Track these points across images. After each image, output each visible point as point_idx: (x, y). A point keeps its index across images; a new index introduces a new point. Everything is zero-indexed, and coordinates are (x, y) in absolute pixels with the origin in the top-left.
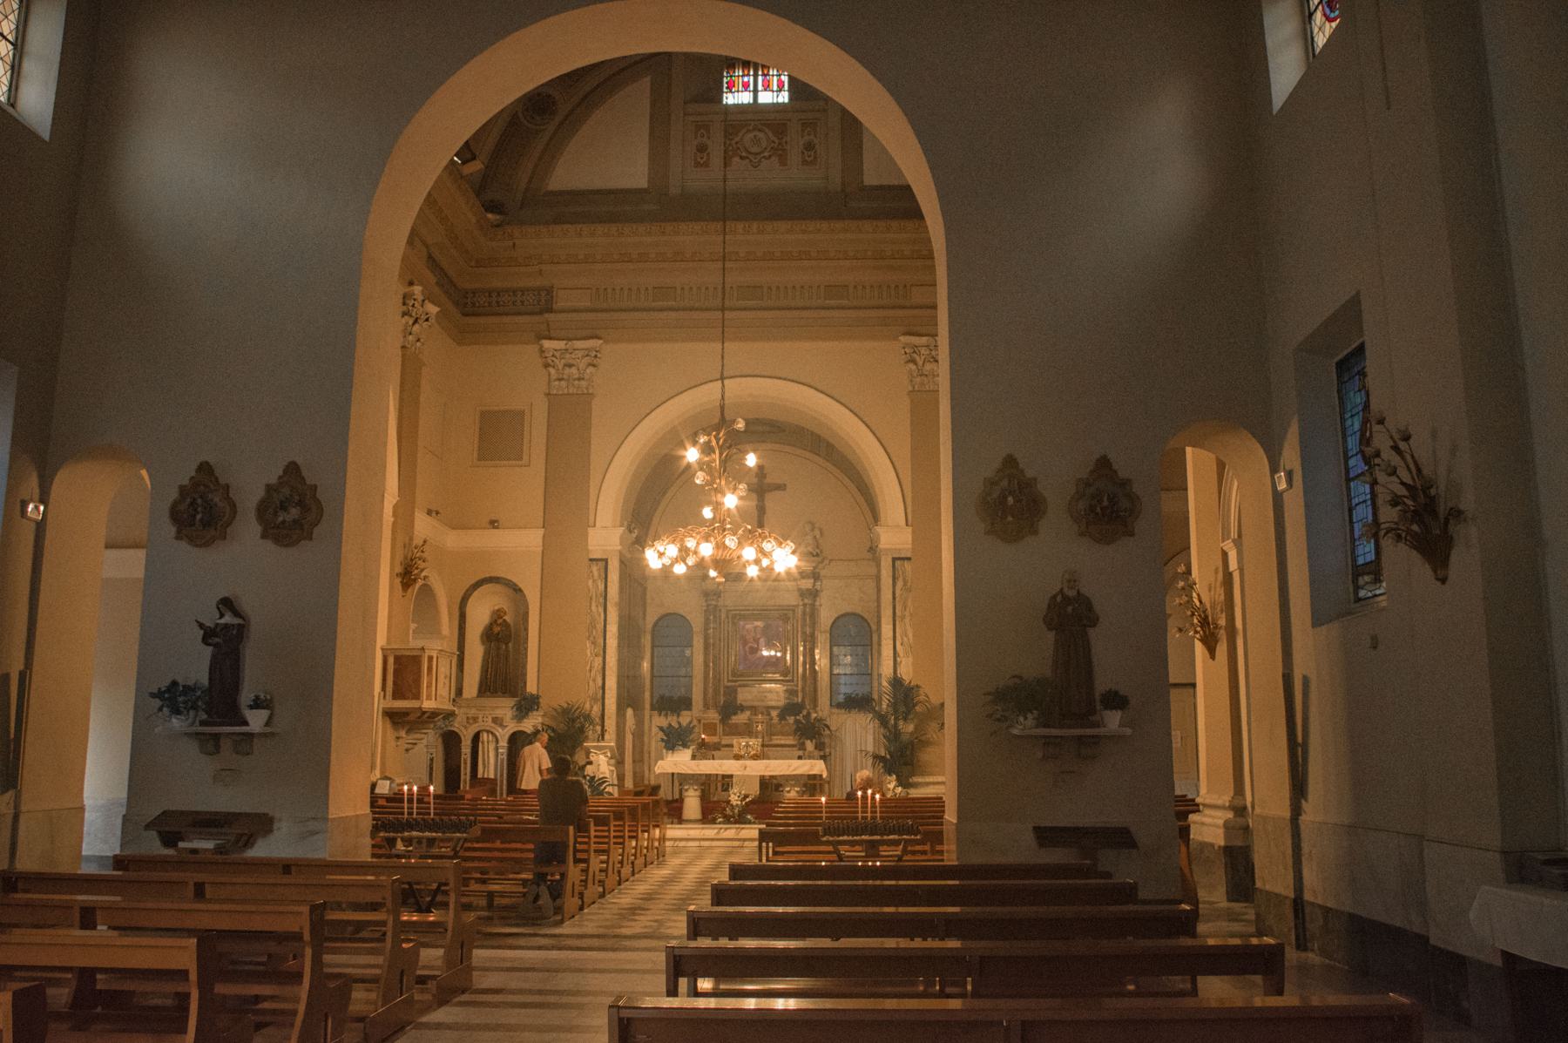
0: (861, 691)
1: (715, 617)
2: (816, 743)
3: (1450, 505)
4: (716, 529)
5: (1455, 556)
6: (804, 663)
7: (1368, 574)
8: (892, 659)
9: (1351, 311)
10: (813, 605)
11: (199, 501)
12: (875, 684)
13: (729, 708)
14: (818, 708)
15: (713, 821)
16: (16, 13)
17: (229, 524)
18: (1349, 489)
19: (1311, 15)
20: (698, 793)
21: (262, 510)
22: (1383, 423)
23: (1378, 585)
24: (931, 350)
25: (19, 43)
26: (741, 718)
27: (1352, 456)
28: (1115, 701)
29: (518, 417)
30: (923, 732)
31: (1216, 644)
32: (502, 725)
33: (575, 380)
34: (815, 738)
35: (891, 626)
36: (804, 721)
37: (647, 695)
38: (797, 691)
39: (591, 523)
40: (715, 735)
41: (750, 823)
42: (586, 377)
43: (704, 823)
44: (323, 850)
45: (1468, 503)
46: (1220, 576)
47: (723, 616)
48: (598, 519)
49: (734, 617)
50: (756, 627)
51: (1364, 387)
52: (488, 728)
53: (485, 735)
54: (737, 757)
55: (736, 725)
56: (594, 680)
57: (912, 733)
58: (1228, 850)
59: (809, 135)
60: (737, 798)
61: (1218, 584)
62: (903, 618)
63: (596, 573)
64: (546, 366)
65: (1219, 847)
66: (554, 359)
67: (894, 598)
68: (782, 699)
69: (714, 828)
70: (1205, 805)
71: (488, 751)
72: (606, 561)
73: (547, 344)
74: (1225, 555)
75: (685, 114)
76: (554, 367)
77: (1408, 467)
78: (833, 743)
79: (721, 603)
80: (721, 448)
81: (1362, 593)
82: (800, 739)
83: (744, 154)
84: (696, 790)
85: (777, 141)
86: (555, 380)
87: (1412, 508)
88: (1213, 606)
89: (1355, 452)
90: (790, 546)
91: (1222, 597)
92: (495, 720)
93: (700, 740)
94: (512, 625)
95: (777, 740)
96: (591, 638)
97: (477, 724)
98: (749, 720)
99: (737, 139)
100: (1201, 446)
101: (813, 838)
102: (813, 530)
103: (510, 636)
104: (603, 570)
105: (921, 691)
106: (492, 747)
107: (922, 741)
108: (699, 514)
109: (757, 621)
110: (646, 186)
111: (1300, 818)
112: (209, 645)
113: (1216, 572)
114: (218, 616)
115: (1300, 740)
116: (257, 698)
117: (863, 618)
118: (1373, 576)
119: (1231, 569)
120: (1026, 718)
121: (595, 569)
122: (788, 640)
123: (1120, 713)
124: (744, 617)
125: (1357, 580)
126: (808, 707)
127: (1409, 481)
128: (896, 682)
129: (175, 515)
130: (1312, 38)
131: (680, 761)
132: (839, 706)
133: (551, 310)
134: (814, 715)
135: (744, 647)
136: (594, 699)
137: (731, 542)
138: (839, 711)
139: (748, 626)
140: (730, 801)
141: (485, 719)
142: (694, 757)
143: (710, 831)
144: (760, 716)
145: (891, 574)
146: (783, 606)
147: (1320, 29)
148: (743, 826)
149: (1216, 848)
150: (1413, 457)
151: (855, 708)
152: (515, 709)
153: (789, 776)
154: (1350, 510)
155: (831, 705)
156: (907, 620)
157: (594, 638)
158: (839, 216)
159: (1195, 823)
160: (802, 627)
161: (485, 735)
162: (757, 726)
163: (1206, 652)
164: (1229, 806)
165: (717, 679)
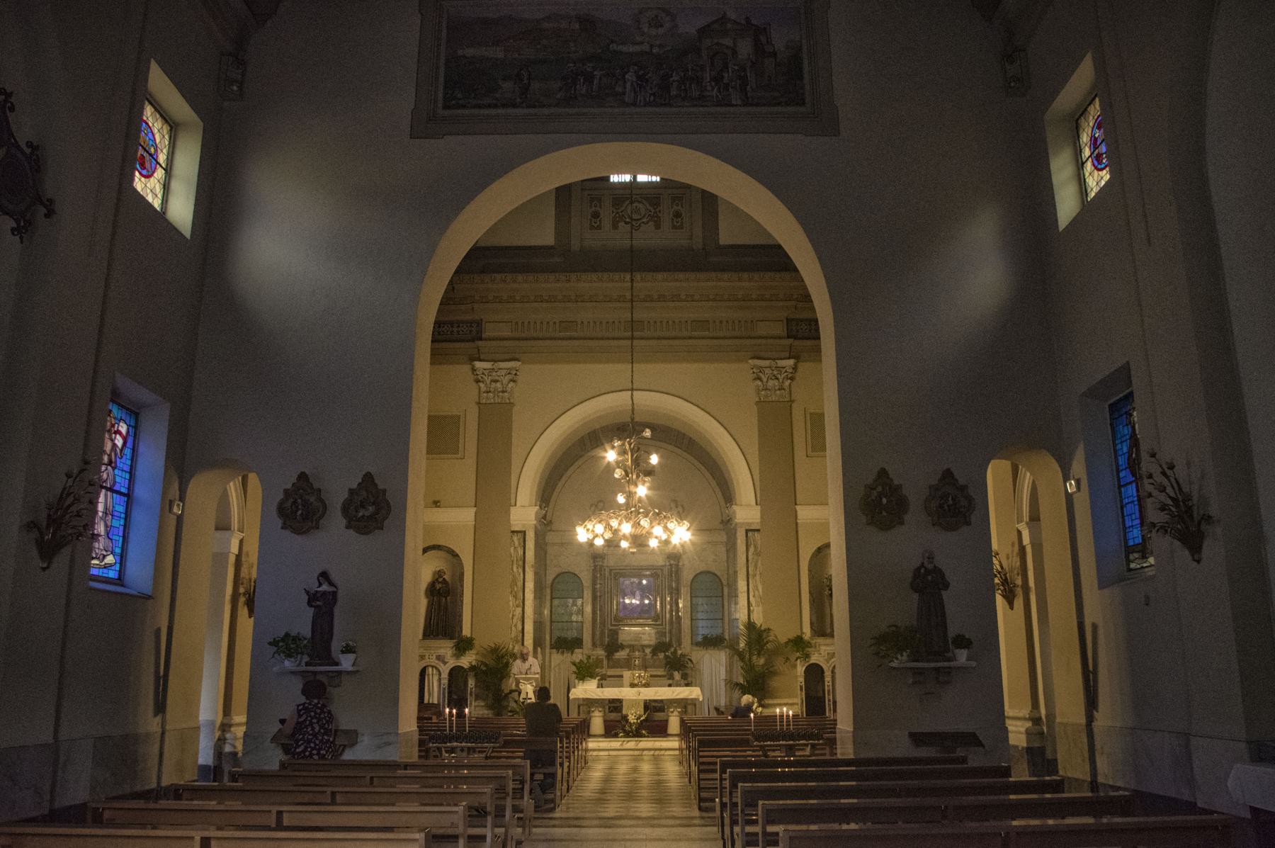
0: (716, 632)
1: (601, 575)
3: (1202, 512)
4: (633, 510)
5: (1207, 545)
6: (671, 611)
7: (1136, 552)
9: (1124, 373)
11: (299, 501)
12: (727, 627)
13: (613, 646)
14: (682, 646)
15: (616, 736)
16: (167, 147)
18: (1120, 493)
19: (1083, 164)
20: (601, 714)
21: (345, 510)
22: (1154, 457)
23: (1145, 560)
24: (773, 370)
25: (169, 169)
26: (622, 654)
27: (1122, 470)
28: (962, 642)
29: (455, 420)
31: (1014, 599)
32: (445, 663)
33: (499, 392)
36: (672, 657)
37: (548, 637)
38: (665, 633)
39: (513, 501)
41: (645, 737)
42: (509, 390)
43: (606, 737)
44: (392, 755)
45: (1214, 510)
46: (1016, 548)
47: (607, 574)
48: (518, 498)
49: (616, 574)
50: (632, 583)
51: (1130, 422)
52: (433, 664)
53: (430, 669)
56: (516, 626)
58: (1029, 750)
59: (678, 206)
60: (633, 717)
61: (1015, 554)
62: (755, 575)
64: (478, 381)
65: (1023, 748)
66: (482, 376)
67: (747, 561)
68: (654, 639)
69: (619, 741)
71: (433, 683)
72: (524, 532)
73: (478, 364)
74: (1019, 533)
75: (582, 189)
76: (483, 382)
77: (1171, 484)
78: (694, 674)
80: (632, 450)
81: (1133, 566)
83: (628, 220)
84: (600, 711)
85: (653, 211)
86: (484, 392)
87: (1176, 514)
89: (1124, 467)
90: (686, 524)
91: (1018, 563)
92: (438, 658)
94: (450, 582)
96: (513, 593)
97: (424, 661)
99: (623, 208)
101: (745, 743)
103: (449, 591)
104: (522, 540)
106: (436, 678)
107: (771, 672)
108: (616, 502)
110: (553, 244)
111: (1093, 724)
112: (312, 606)
113: (1013, 544)
114: (317, 584)
115: (1091, 668)
116: (348, 645)
118: (1141, 554)
119: (1025, 543)
120: (902, 656)
121: (515, 539)
122: (659, 594)
123: (967, 650)
124: (623, 575)
125: (1129, 556)
127: (1172, 494)
128: (750, 626)
129: (281, 510)
130: (1085, 180)
131: (587, 689)
132: (698, 644)
133: (481, 339)
134: (679, 652)
137: (645, 522)
138: (698, 648)
139: (627, 582)
141: (431, 657)
143: (615, 743)
144: (637, 653)
147: (1090, 174)
148: (641, 739)
149: (1020, 749)
150: (1176, 479)
152: (454, 648)
153: (674, 699)
154: (1122, 508)
156: (758, 577)
157: (516, 592)
158: (699, 270)
161: (430, 669)
163: (1006, 603)
164: (1029, 717)
165: (603, 623)
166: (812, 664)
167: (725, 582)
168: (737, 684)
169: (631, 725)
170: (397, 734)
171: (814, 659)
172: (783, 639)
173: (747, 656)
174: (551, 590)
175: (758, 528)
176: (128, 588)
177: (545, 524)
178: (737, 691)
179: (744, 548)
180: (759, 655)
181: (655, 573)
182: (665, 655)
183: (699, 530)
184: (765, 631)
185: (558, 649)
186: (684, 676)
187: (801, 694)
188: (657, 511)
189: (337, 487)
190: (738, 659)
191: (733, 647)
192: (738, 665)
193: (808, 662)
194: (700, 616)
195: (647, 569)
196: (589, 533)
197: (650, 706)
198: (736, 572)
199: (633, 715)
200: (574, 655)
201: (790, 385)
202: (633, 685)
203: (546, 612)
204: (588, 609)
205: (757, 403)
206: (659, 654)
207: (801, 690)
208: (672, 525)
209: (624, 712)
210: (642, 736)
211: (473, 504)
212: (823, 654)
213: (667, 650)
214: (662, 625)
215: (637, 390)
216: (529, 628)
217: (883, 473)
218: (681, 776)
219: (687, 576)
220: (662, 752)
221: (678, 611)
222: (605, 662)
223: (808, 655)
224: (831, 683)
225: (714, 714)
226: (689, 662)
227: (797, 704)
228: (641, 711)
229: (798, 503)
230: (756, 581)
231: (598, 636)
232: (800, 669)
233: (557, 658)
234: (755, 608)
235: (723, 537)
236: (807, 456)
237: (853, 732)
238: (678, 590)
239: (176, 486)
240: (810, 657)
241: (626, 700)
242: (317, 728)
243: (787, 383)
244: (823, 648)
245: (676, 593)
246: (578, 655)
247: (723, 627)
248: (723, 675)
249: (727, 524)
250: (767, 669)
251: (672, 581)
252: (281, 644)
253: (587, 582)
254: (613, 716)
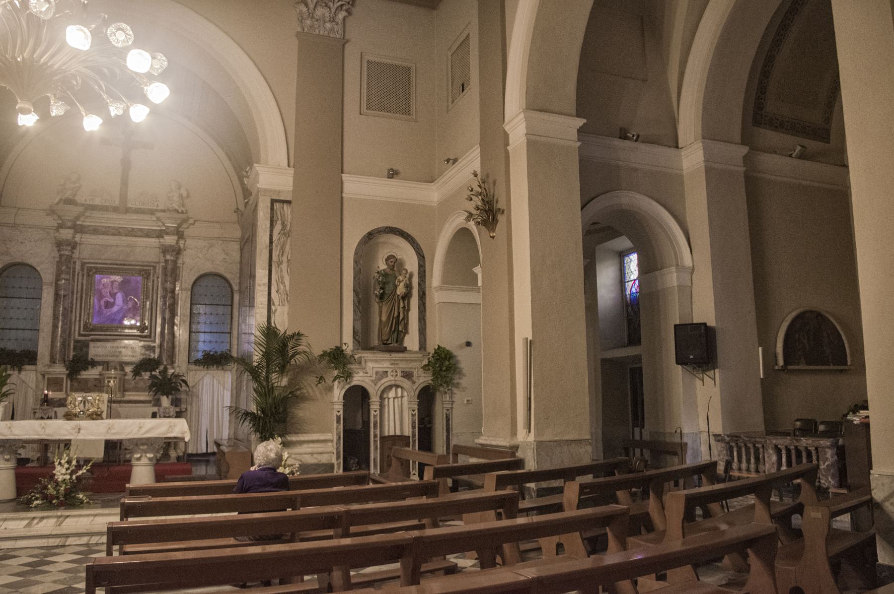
0: (221, 348)
2: (172, 399)
8: (266, 307)
10: (175, 262)
12: (235, 341)
14: (176, 365)
26: (92, 373)
30: (297, 387)
34: (172, 394)
35: (267, 272)
36: (160, 377)
40: (61, 390)
47: (78, 267)
49: (90, 269)
50: (113, 282)
54: (69, 416)
60: (64, 471)
62: (280, 263)
67: (271, 242)
69: (23, 519)
78: (189, 400)
82: (155, 395)
84: (7, 460)
93: (43, 396)
95: (130, 396)
98: (100, 375)
105: (304, 341)
107: (297, 397)
109: (115, 275)
126: (165, 363)
128: (270, 332)
132: (197, 362)
134: (171, 371)
135: (99, 301)
138: (197, 367)
140: (54, 475)
144: (113, 372)
145: (269, 216)
146: (144, 262)
151: (213, 365)
153: (141, 439)
155: (189, 362)
156: (284, 266)
160: (163, 284)
162: (109, 382)
166: (355, 386)
167: (236, 288)
168: (247, 414)
171: (358, 379)
172: (317, 352)
178: (247, 423)
182: (151, 374)
184: (293, 336)
186: (176, 402)
187: (337, 428)
190: (251, 378)
192: (249, 386)
193: (349, 383)
194: (201, 327)
200: (23, 373)
201: (344, 19)
205: (298, 35)
206: (143, 373)
207: (338, 421)
210: (79, 505)
212: (370, 373)
214: (150, 336)
223: (350, 373)
224: (378, 412)
226: (183, 384)
227: (332, 441)
229: (344, 171)
230: (281, 271)
232: (338, 393)
234: (279, 309)
236: (360, 114)
240: (352, 377)
243: (341, 15)
244: (370, 365)
248: (228, 403)
250: (290, 393)
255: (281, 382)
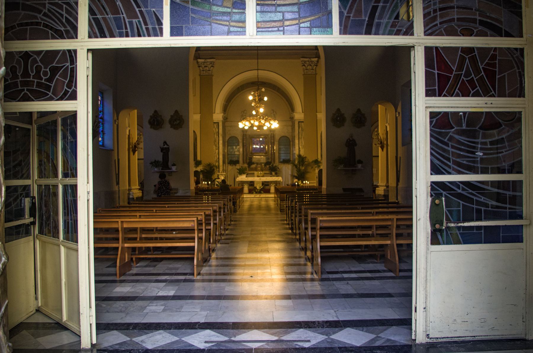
4: (258, 117)
6: (271, 150)
12: (291, 156)
13: (250, 163)
15: (253, 193)
17: (163, 124)
20: (247, 186)
21: (170, 122)
26: (253, 166)
28: (360, 162)
39: (214, 112)
42: (211, 70)
46: (385, 132)
47: (248, 137)
49: (251, 137)
55: (252, 168)
56: (216, 156)
57: (304, 170)
62: (301, 138)
63: (216, 127)
64: (199, 67)
70: (380, 186)
72: (218, 123)
73: (199, 60)
74: (386, 127)
79: (247, 133)
80: (258, 96)
88: (383, 138)
90: (277, 122)
100: (382, 105)
102: (274, 112)
105: (307, 158)
113: (384, 130)
115: (399, 170)
116: (174, 164)
117: (288, 137)
121: (215, 125)
124: (253, 137)
128: (299, 156)
131: (243, 178)
132: (281, 162)
134: (274, 165)
136: (216, 161)
137: (263, 121)
139: (255, 140)
142: (246, 177)
143: (252, 196)
156: (302, 139)
159: (377, 190)
165: (247, 155)
167: (291, 140)
169: (258, 190)
170: (190, 189)
172: (311, 160)
173: (298, 166)
174: (228, 143)
175: (303, 121)
176: (105, 147)
177: (225, 119)
179: (298, 128)
180: (302, 166)
181: (266, 136)
183: (288, 297)
185: (230, 164)
186: (276, 174)
188: (267, 117)
189: (167, 114)
191: (293, 163)
194: (282, 152)
195: (263, 135)
196: (244, 125)
197: (265, 184)
198: (295, 136)
199: (258, 186)
201: (316, 68)
202: (258, 176)
203: (226, 151)
204: (241, 150)
207: (317, 178)
208: (272, 122)
209: (255, 186)
211: (199, 113)
213: (270, 165)
214: (268, 155)
215: (259, 70)
216: (221, 157)
217: (338, 110)
218: (275, 204)
219: (277, 138)
220: (268, 198)
221: (274, 150)
222: (248, 169)
225: (286, 186)
228: (261, 185)
229: (318, 111)
231: (245, 160)
232: (317, 171)
233: (230, 167)
235: (290, 123)
237: (326, 188)
238: (274, 143)
239: (116, 116)
241: (256, 181)
242: (164, 188)
243: (315, 67)
245: (273, 144)
246: (238, 166)
247: (290, 156)
248: (290, 173)
249: (292, 119)
251: (272, 139)
252: (154, 163)
253: (240, 140)
254: (251, 187)
255: (303, 168)
